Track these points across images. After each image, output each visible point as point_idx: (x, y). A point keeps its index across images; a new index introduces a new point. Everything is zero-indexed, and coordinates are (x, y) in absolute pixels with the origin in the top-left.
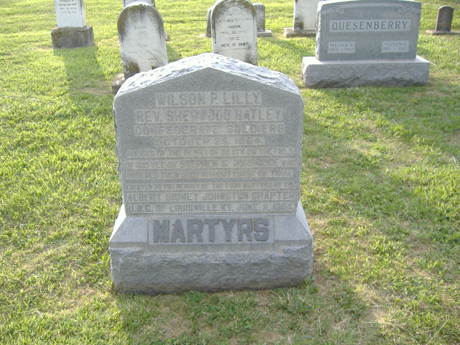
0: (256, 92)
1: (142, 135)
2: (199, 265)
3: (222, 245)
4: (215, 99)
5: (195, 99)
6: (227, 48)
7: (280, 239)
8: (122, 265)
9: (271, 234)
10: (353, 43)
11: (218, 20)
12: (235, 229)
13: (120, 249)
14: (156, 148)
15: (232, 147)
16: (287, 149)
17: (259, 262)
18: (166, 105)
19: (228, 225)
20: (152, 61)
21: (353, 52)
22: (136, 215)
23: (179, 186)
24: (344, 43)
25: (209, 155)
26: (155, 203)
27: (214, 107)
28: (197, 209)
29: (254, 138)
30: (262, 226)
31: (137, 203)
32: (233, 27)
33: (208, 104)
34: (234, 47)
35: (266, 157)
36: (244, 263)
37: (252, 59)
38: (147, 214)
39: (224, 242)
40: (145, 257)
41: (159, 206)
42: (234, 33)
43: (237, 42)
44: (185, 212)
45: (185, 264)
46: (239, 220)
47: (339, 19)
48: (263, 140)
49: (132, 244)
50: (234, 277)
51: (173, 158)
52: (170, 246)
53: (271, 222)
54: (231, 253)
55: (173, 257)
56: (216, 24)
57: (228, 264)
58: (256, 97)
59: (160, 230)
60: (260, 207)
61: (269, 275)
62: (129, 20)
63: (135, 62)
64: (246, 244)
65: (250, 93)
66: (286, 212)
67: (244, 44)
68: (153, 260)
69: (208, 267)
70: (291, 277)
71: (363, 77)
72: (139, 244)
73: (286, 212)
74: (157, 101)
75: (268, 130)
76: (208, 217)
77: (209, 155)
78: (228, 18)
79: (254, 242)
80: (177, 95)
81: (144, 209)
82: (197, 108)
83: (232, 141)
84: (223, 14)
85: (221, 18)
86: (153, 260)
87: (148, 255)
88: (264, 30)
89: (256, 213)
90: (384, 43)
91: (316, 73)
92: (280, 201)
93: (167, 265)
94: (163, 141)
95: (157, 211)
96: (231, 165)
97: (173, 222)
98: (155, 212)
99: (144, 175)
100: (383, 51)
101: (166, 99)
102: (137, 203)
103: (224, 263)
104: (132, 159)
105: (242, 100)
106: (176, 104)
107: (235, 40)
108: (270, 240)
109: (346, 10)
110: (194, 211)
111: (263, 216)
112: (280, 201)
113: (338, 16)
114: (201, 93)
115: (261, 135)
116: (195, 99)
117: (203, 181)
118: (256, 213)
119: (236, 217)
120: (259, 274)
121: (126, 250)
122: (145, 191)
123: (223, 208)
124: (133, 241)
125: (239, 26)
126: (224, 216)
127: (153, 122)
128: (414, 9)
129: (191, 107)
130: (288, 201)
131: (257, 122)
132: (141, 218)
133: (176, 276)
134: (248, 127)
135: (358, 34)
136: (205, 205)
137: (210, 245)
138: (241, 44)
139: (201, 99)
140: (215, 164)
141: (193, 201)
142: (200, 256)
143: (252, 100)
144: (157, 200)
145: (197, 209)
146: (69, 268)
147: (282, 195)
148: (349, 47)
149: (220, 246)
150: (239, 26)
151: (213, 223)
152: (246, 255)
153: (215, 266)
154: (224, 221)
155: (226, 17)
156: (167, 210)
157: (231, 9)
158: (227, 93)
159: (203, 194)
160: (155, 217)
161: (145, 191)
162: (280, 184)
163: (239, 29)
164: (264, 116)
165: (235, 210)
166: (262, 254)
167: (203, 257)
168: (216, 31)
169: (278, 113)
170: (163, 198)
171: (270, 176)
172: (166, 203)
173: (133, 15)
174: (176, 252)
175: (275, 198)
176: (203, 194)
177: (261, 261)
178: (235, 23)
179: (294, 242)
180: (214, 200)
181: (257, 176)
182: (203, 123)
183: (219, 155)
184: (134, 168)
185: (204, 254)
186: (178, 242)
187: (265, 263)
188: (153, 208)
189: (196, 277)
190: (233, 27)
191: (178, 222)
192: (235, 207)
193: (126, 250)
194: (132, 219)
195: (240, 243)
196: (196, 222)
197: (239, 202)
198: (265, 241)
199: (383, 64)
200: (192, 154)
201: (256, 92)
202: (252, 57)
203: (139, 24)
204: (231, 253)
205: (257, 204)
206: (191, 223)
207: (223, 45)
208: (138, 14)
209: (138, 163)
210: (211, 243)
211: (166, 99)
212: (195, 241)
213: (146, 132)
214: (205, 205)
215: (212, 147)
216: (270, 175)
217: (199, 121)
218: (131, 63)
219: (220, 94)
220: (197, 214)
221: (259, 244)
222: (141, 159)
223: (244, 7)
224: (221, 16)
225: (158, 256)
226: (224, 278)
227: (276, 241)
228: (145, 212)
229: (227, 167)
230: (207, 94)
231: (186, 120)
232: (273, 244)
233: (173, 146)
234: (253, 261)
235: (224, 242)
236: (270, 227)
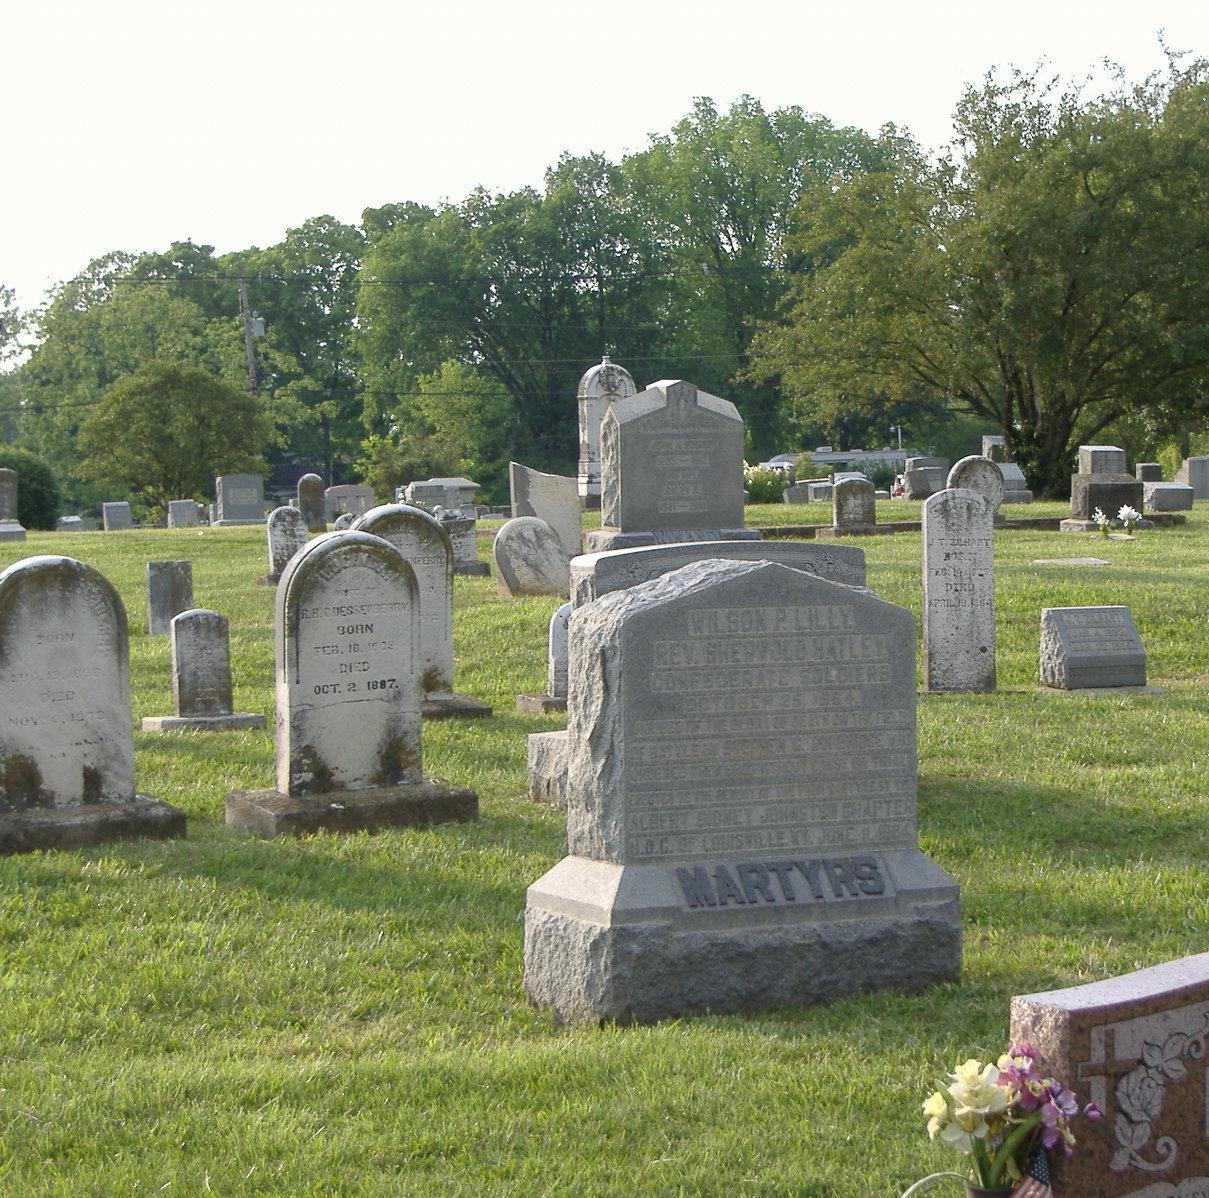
0: (844, 608)
1: (664, 691)
2: (776, 949)
3: (810, 905)
4: (782, 620)
5: (751, 622)
6: (331, 697)
7: (907, 888)
8: (640, 957)
9: (887, 882)
11: (308, 607)
12: (823, 876)
13: (631, 925)
14: (685, 717)
15: (809, 711)
16: (897, 713)
17: (879, 936)
18: (706, 632)
19: (809, 872)
20: (87, 748)
22: (643, 861)
23: (721, 794)
25: (772, 729)
26: (677, 834)
27: (781, 635)
28: (749, 842)
29: (844, 693)
30: (867, 869)
31: (645, 836)
32: (352, 630)
33: (771, 629)
34: (352, 696)
35: (863, 730)
36: (852, 940)
37: (405, 733)
38: (662, 859)
39: (812, 900)
40: (679, 940)
41: (684, 839)
42: (354, 647)
43: (361, 678)
44: (729, 851)
45: (750, 949)
46: (825, 862)
48: (857, 695)
49: (652, 912)
50: (834, 977)
51: (713, 737)
52: (719, 913)
53: (880, 863)
54: (827, 923)
55: (727, 935)
56: (302, 622)
57: (825, 945)
58: (846, 616)
59: (692, 883)
60: (856, 835)
61: (896, 968)
62: (24, 610)
63: (27, 753)
64: (851, 902)
65: (835, 610)
66: (902, 843)
67: (383, 684)
68: (693, 944)
69: (790, 953)
70: (932, 970)
72: (667, 912)
73: (902, 843)
74: (691, 626)
75: (865, 677)
76: (769, 858)
77: (772, 729)
78: (337, 600)
79: (863, 896)
80: (722, 613)
81: (657, 848)
82: (753, 637)
83: (809, 701)
84: (323, 589)
85: (319, 600)
86: (693, 944)
87: (683, 935)
88: (230, 709)
89: (851, 847)
92: (889, 820)
93: (718, 953)
94: (698, 701)
95: (681, 851)
96: (807, 747)
97: (711, 871)
98: (676, 853)
99: (662, 774)
101: (706, 621)
102: (645, 836)
103: (817, 943)
104: (644, 740)
105: (824, 622)
106: (723, 631)
107: (355, 672)
108: (889, 893)
110: (745, 849)
111: (863, 852)
112: (889, 820)
114: (761, 610)
115: (854, 688)
116: (751, 622)
117: (761, 781)
118: (851, 847)
119: (818, 856)
120: (878, 966)
121: (644, 925)
122: (663, 809)
123: (795, 841)
124: (655, 905)
125: (369, 628)
126: (797, 857)
127: (684, 665)
128: (846, 567)
129: (744, 637)
130: (902, 820)
131: (848, 663)
132: (653, 867)
133: (732, 981)
134: (834, 673)
136: (764, 833)
137: (789, 907)
139: (761, 622)
140: (782, 746)
141: (745, 825)
142: (774, 931)
143: (838, 621)
144: (682, 828)
145: (749, 842)
147: (892, 806)
149: (806, 909)
150: (369, 628)
151: (782, 870)
152: (851, 926)
153: (801, 950)
154: (798, 865)
155: (331, 597)
156: (698, 850)
158: (802, 610)
159: (760, 811)
160: (677, 864)
161: (663, 809)
162: (887, 783)
164: (858, 651)
165: (816, 844)
166: (883, 921)
167: (781, 934)
168: (301, 643)
169: (878, 645)
170: (692, 822)
171: (872, 768)
172: (696, 832)
173: (37, 596)
175: (882, 814)
176: (760, 811)
177: (882, 933)
178: (356, 619)
179: (928, 893)
180: (779, 823)
181: (850, 769)
182: (763, 666)
183: (788, 727)
184: (646, 758)
185: (780, 929)
186: (732, 904)
187: (889, 937)
188: (673, 845)
189: (766, 983)
190: (352, 630)
191: (721, 870)
192: (815, 835)
193: (644, 925)
194: (636, 869)
195: (839, 900)
196: (754, 869)
197: (821, 824)
198: (881, 893)
200: (744, 726)
201: (844, 608)
202: (405, 726)
203: (54, 623)
204: (827, 923)
205: (851, 829)
206: (745, 870)
207: (319, 690)
208: (54, 593)
209: (654, 747)
210: (790, 903)
211: (706, 621)
212: (762, 902)
213: (671, 685)
214: (764, 833)
215: (778, 712)
216: (870, 766)
217: (756, 661)
218: (15, 757)
219: (790, 611)
220: (750, 854)
221: (871, 901)
222: (660, 739)
223: (387, 568)
225: (697, 936)
226: (816, 981)
227: (901, 893)
228: (659, 855)
229: (801, 753)
230: (770, 613)
231: (737, 660)
232: (896, 900)
233: (713, 711)
234: (867, 935)
235: (812, 900)
236: (881, 870)
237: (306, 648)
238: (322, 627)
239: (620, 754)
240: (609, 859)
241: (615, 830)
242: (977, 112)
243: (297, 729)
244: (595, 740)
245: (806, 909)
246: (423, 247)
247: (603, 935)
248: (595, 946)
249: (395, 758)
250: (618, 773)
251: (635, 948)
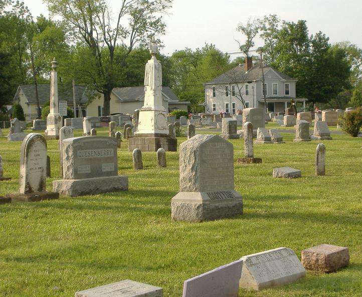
6: (32, 171)
10: (89, 166)
21: (90, 172)
24: (85, 166)
34: (35, 171)
43: (37, 167)
47: (82, 149)
71: (100, 188)
90: (103, 165)
91: (79, 187)
100: (103, 171)
109: (84, 143)
113: (81, 148)
135: (91, 159)
138: (39, 168)
146: (34, 122)
148: (86, 169)
149: (224, 200)
155: (33, 148)
157: (36, 143)
163: (39, 157)
174: (14, 96)
178: (37, 153)
199: (108, 178)
224: (31, 147)
237: (29, 160)
238: (32, 155)
239: (198, 171)
240: (196, 190)
241: (197, 185)
242: (319, 35)
243: (27, 178)
244: (192, 169)
245: (224, 200)
246: (287, 31)
247: (200, 205)
248: (198, 207)
249: (42, 185)
250: (198, 175)
251: (206, 207)
